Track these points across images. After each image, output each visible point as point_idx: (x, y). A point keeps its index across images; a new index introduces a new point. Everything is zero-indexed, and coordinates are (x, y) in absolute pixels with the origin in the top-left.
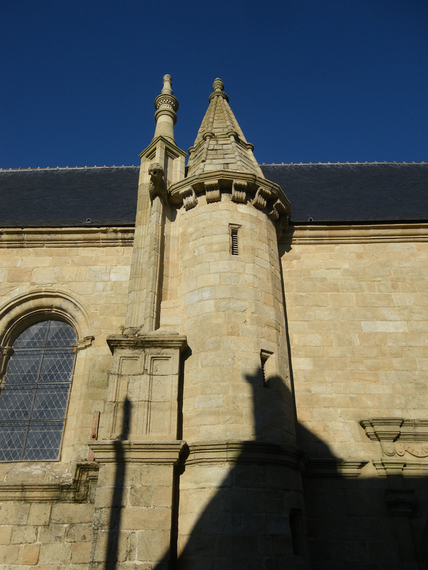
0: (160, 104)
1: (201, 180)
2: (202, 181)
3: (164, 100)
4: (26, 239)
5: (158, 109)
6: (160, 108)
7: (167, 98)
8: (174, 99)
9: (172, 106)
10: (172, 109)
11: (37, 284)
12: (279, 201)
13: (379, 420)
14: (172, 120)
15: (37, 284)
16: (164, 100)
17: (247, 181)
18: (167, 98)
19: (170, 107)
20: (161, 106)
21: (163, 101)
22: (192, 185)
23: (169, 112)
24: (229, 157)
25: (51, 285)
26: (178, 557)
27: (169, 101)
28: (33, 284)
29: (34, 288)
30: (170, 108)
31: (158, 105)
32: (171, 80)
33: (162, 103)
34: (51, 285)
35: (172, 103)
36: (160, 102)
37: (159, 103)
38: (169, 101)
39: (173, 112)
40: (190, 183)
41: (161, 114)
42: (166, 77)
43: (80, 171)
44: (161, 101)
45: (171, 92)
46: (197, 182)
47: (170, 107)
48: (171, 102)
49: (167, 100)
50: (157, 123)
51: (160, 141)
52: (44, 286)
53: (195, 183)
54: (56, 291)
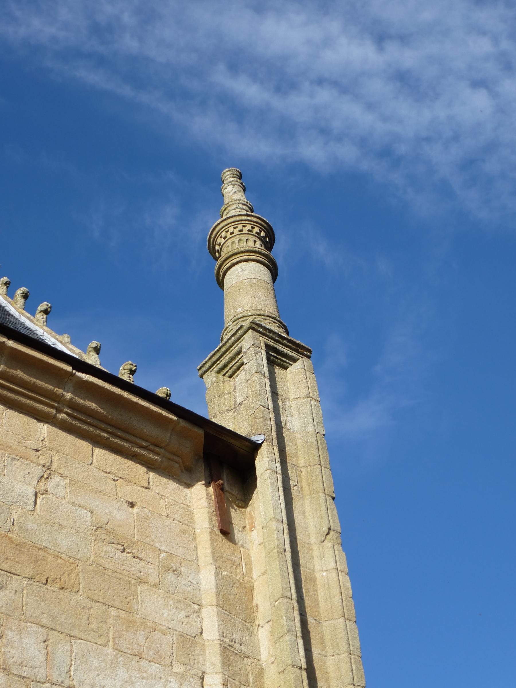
3: (240, 227)
4: (302, 366)
5: (220, 256)
6: (223, 254)
8: (264, 224)
9: (262, 239)
10: (261, 246)
14: (270, 275)
16: (231, 230)
19: (255, 242)
23: (261, 256)
27: (253, 228)
31: (217, 248)
33: (232, 233)
35: (263, 234)
37: (219, 241)
38: (253, 228)
39: (262, 261)
43: (70, 410)
44: (224, 234)
47: (255, 242)
48: (261, 232)
50: (223, 290)
51: (250, 330)
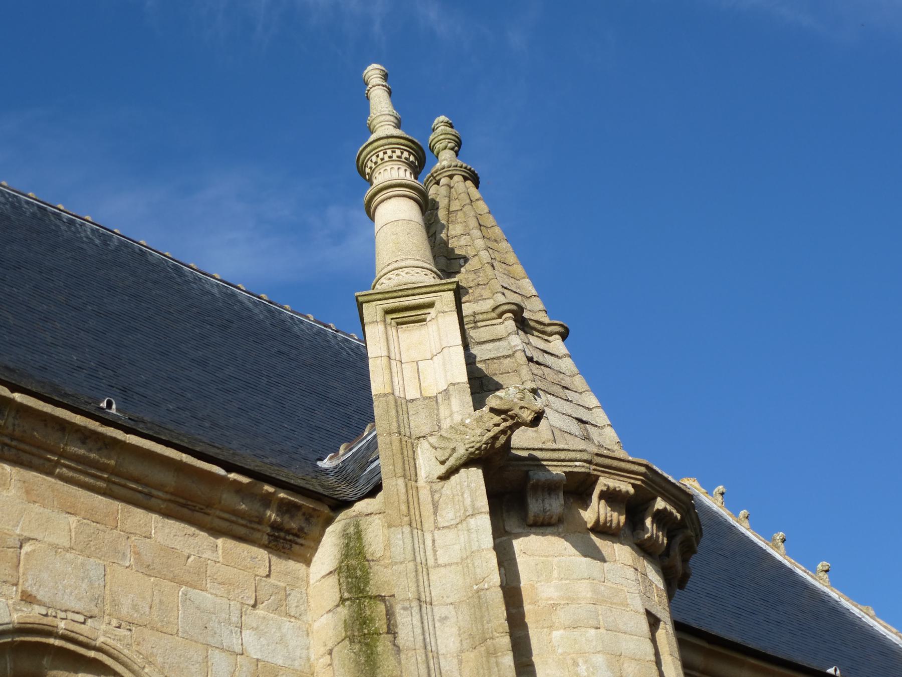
0: (371, 168)
1: (594, 470)
2: (595, 473)
6: (375, 182)
7: (387, 147)
11: (40, 603)
12: (660, 504)
13: (447, 291)
15: (40, 603)
16: (381, 154)
17: (632, 481)
18: (387, 147)
20: (376, 174)
21: (378, 156)
22: (568, 470)
24: (477, 599)
25: (81, 618)
26: (601, 524)
28: (28, 598)
29: (32, 614)
30: (402, 171)
32: (385, 77)
33: (376, 163)
34: (81, 618)
35: (406, 154)
36: (371, 161)
40: (563, 464)
41: (379, 199)
42: (373, 73)
45: (394, 125)
46: (583, 470)
49: (389, 152)
52: (63, 615)
53: (576, 470)
54: (98, 643)
